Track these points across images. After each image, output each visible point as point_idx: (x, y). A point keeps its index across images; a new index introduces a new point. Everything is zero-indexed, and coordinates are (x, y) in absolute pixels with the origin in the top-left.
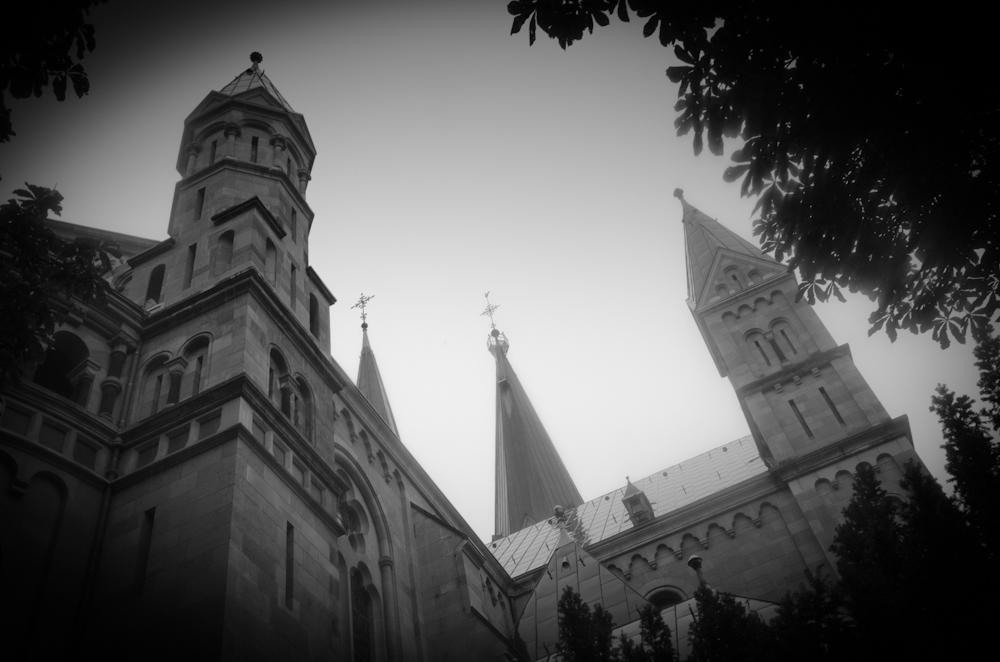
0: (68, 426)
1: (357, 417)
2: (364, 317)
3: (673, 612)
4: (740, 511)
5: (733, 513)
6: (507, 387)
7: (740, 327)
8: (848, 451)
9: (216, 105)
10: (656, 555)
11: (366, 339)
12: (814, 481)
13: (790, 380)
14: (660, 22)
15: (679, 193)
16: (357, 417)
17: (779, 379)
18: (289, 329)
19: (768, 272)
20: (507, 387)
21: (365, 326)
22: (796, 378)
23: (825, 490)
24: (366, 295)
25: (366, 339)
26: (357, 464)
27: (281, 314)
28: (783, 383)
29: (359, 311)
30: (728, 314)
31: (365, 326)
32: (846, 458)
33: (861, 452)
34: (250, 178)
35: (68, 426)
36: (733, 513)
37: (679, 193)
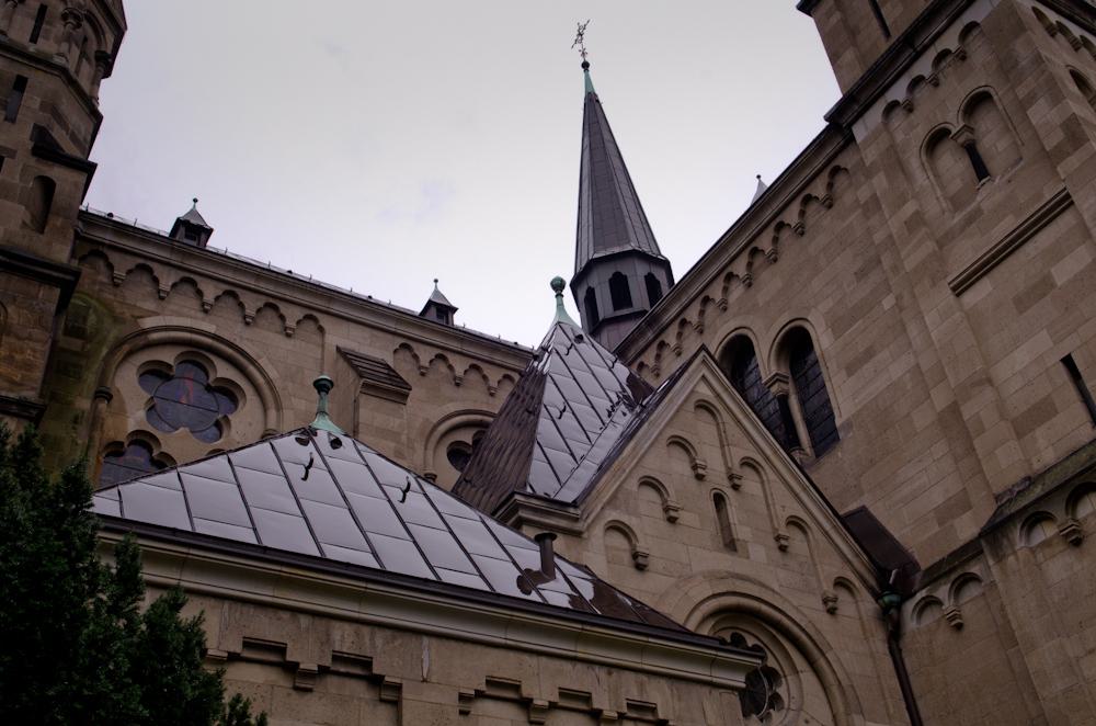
0: (619, 313)
1: (772, 653)
4: (445, 353)
5: (403, 341)
6: (592, 104)
10: (259, 311)
11: (588, 82)
12: (565, 279)
14: (891, 582)
15: (759, 177)
16: (772, 653)
20: (592, 104)
21: (585, 66)
23: (898, 118)
24: (582, 24)
25: (588, 82)
29: (578, 46)
31: (585, 66)
35: (619, 313)
36: (403, 341)
37: (759, 177)
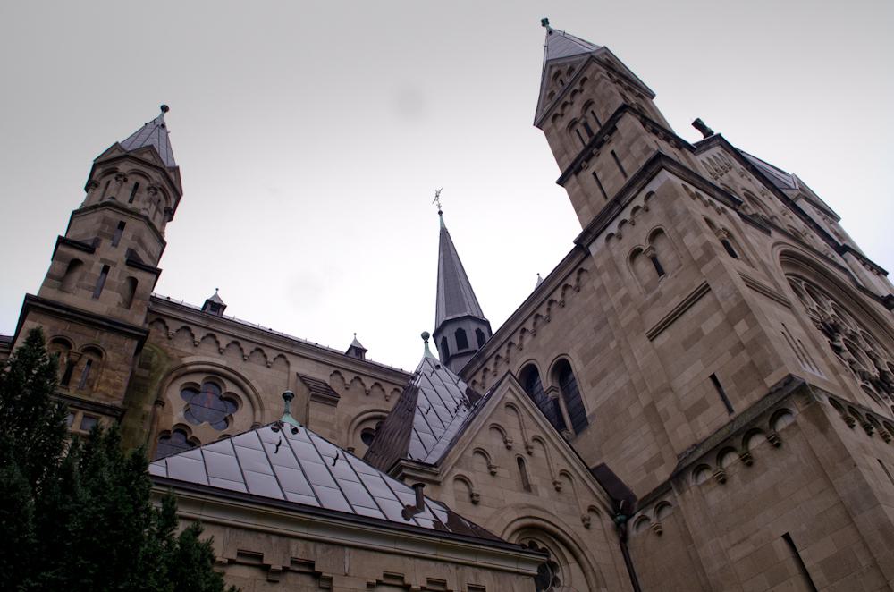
2: (439, 207)
3: (514, 374)
6: (444, 234)
7: (563, 124)
8: (623, 202)
9: (116, 154)
11: (442, 222)
13: (591, 156)
15: (545, 22)
17: (583, 158)
18: (76, 319)
19: (577, 64)
20: (444, 234)
21: (440, 213)
22: (595, 151)
26: (225, 368)
27: (64, 312)
28: (588, 160)
29: (436, 203)
30: (556, 116)
31: (440, 213)
32: (623, 208)
33: (633, 198)
34: (88, 216)
36: (576, 271)
